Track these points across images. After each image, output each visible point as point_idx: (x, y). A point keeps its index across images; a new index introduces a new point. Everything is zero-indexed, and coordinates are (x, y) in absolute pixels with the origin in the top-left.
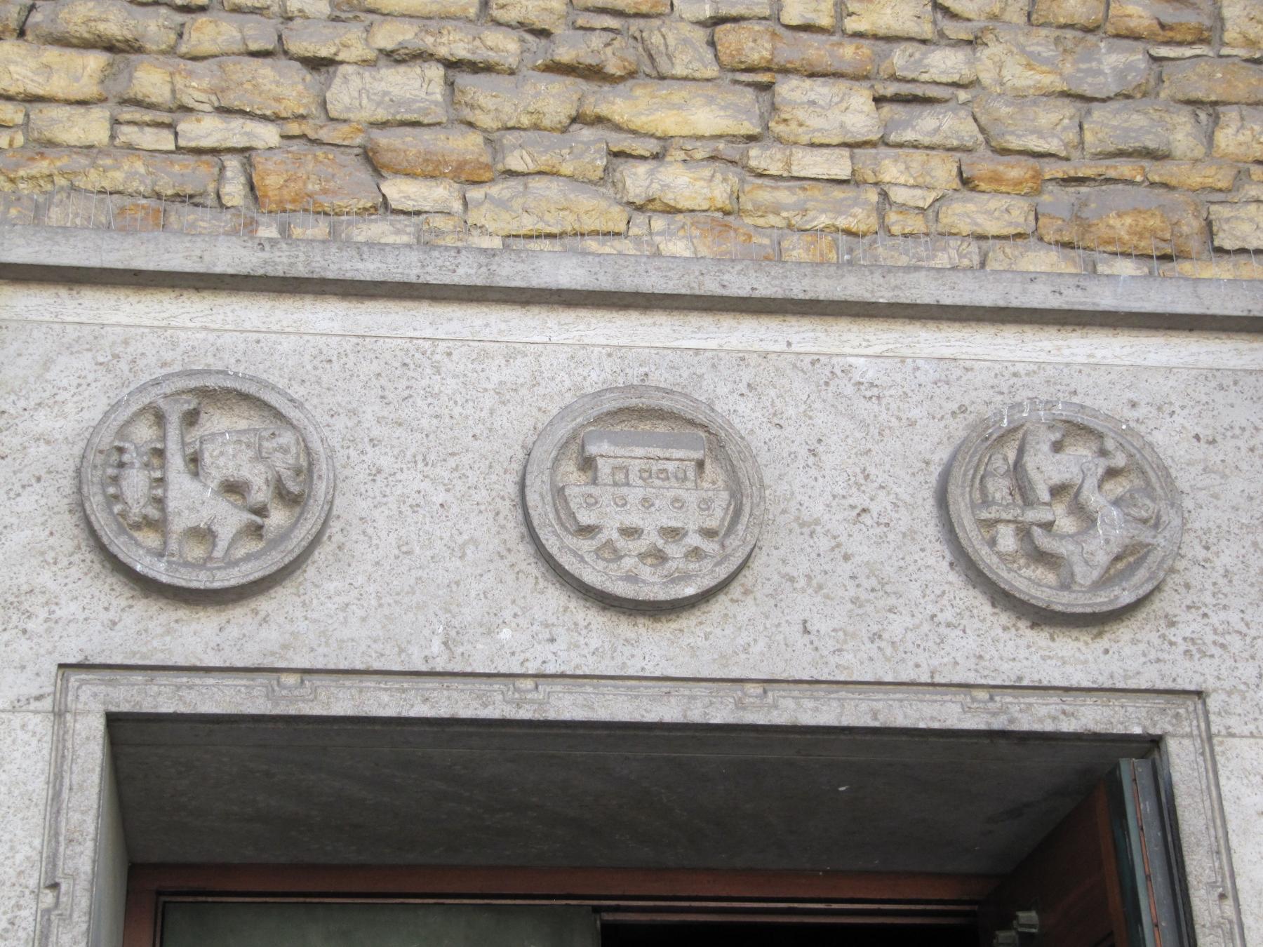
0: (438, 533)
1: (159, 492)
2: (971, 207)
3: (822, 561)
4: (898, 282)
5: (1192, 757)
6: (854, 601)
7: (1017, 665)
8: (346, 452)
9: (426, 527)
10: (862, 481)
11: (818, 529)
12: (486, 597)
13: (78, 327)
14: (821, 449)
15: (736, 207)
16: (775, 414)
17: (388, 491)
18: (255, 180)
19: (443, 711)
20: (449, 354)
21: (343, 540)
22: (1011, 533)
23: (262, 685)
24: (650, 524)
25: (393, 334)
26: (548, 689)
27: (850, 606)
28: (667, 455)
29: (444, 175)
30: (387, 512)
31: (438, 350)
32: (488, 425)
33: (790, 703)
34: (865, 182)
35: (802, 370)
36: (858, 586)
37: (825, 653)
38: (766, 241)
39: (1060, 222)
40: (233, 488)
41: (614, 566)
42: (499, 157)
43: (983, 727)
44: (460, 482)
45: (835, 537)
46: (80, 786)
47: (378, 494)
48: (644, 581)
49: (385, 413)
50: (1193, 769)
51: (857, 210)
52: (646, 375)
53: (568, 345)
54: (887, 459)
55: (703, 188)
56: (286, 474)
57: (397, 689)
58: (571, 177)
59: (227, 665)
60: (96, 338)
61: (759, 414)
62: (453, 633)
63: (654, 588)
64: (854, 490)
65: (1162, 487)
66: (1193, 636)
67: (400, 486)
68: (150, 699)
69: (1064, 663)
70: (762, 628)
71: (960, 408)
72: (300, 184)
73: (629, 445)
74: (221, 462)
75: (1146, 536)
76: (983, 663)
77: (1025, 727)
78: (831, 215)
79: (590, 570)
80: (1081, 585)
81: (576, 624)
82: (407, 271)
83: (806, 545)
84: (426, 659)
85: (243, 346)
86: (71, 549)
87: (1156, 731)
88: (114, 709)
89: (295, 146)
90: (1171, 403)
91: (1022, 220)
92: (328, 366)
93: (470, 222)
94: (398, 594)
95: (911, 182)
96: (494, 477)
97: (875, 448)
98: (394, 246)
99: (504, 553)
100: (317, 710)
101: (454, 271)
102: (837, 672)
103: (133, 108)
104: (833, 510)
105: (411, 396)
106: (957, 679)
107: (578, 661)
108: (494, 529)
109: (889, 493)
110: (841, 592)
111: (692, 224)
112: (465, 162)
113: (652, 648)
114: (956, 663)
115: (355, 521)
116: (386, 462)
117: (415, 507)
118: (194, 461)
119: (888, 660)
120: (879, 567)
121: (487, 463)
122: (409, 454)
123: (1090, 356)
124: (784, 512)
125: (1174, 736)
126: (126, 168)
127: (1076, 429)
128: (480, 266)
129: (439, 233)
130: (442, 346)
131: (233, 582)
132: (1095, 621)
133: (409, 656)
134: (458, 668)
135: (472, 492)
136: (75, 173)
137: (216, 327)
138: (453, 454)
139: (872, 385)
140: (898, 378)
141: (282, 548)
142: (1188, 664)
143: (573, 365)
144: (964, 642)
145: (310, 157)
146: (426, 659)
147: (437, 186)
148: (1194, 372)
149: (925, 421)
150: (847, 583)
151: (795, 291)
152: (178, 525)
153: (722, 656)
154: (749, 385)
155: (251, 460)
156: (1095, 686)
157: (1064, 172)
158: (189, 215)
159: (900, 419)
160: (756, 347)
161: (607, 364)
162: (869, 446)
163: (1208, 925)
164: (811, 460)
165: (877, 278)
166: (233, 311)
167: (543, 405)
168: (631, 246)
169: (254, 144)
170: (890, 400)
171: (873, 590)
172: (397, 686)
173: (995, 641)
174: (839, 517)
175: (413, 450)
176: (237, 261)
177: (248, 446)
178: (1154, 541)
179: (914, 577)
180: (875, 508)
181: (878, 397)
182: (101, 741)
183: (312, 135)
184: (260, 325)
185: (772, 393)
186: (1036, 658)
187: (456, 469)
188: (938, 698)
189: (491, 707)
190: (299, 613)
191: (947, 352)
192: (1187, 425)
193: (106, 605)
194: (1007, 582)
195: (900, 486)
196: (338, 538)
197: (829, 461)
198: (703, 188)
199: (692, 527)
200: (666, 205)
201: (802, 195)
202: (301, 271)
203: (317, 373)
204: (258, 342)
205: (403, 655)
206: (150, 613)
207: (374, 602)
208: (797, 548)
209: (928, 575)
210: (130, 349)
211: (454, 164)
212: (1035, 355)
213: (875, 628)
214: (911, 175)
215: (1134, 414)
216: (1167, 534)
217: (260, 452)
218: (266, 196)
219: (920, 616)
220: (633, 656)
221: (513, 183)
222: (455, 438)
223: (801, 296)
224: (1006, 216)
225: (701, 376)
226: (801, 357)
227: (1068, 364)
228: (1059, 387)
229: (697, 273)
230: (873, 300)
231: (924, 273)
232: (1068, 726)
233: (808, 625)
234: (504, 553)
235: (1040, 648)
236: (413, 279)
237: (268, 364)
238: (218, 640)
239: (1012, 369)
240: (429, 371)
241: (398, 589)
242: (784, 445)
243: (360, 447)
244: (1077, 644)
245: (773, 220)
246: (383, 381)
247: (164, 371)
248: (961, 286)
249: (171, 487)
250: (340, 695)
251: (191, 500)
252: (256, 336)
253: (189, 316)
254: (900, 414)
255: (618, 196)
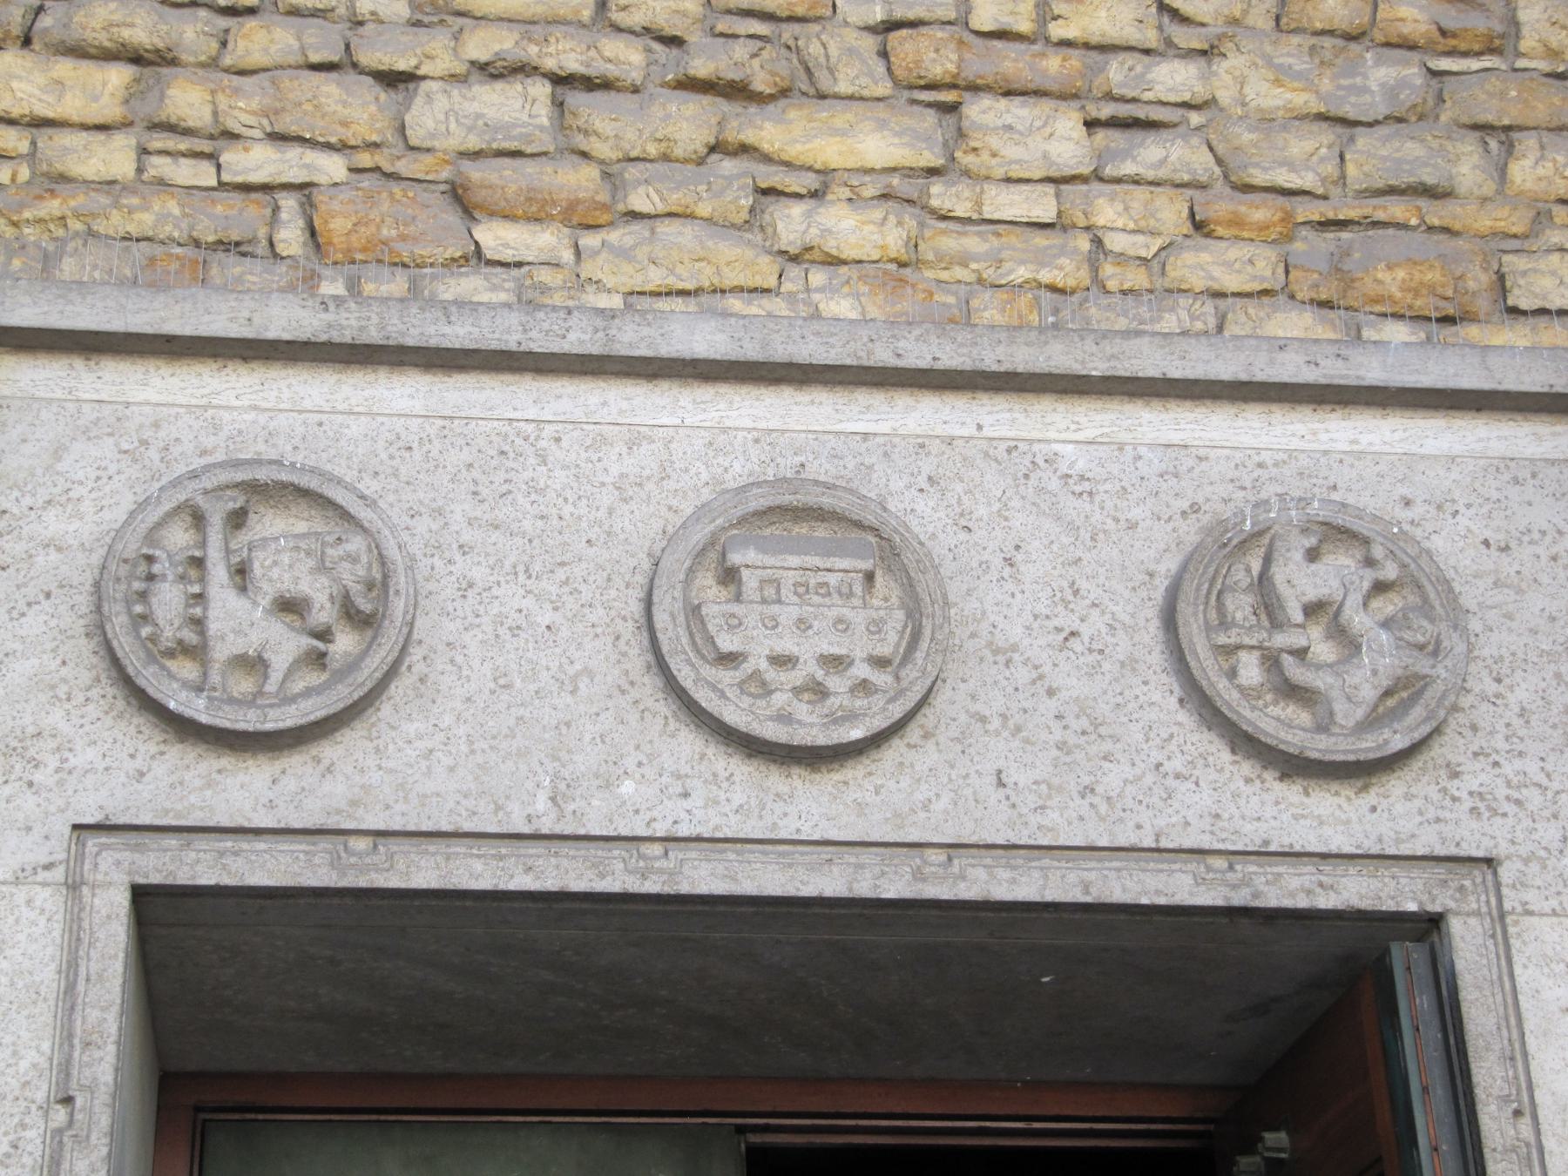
0: (544, 662)
1: (198, 611)
2: (1205, 257)
3: (1020, 696)
4: (1115, 350)
5: (1480, 940)
6: (1061, 746)
7: (1263, 826)
8: (429, 561)
9: (529, 655)
10: (1071, 598)
11: (1016, 656)
12: (603, 742)
13: (97, 406)
14: (1019, 557)
15: (913, 257)
16: (962, 515)
17: (482, 610)
18: (316, 224)
19: (550, 883)
20: (558, 440)
21: (426, 670)
22: (1256, 662)
23: (325, 851)
24: (807, 650)
25: (488, 414)
26: (681, 856)
27: (1055, 753)
28: (828, 566)
29: (551, 218)
30: (480, 636)
31: (544, 435)
32: (606, 527)
33: (981, 873)
34: (1074, 226)
35: (996, 460)
36: (1065, 727)
37: (1025, 811)
38: (951, 300)
39: (1316, 276)
40: (289, 606)
41: (762, 703)
42: (620, 195)
43: (1220, 902)
44: (571, 599)
45: (1036, 667)
46: (100, 976)
47: (469, 614)
48: (799, 722)
49: (478, 513)
50: (1481, 955)
51: (1064, 261)
52: (803, 465)
53: (705, 428)
54: (1101, 570)
55: (872, 233)
56: (356, 589)
57: (493, 856)
58: (709, 220)
59: (282, 825)
60: (119, 419)
61: (942, 514)
62: (562, 786)
63: (812, 730)
64: (1060, 608)
65: (1442, 605)
66: (1482, 789)
67: (496, 603)
68: (186, 868)
69: (1321, 823)
70: (945, 780)
71: (1191, 506)
72: (373, 229)
73: (781, 552)
74: (275, 573)
75: (1423, 666)
76: (1221, 824)
77: (1272, 902)
78: (1032, 267)
79: (732, 708)
80: (1342, 727)
81: (715, 775)
82: (505, 337)
83: (1000, 677)
84: (529, 818)
85: (302, 429)
86: (89, 682)
87: (1436, 908)
88: (141, 881)
89: (367, 182)
90: (1454, 501)
91: (1268, 273)
92: (407, 455)
93: (583, 276)
94: (494, 738)
95: (1132, 226)
96: (613, 593)
97: (1087, 556)
98: (490, 306)
99: (626, 687)
100: (394, 882)
101: (564, 337)
102: (1039, 834)
103: (165, 135)
104: (1035, 634)
105: (510, 492)
106: (1188, 843)
107: (716, 820)
108: (614, 657)
109: (1103, 613)
110: (1044, 735)
111: (860, 278)
112: (578, 202)
113: (810, 804)
114: (1187, 824)
115: (441, 647)
116: (479, 574)
117: (515, 630)
118: (241, 573)
119: (1102, 819)
120: (1092, 704)
121: (605, 574)
122: (508, 564)
123: (1353, 442)
124: (973, 635)
125: (1457, 914)
126: (156, 208)
127: (1336, 533)
128: (596, 331)
129: (545, 289)
130: (549, 430)
131: (289, 723)
132: (1360, 772)
133: (508, 814)
134: (568, 830)
135: (586, 610)
136: (93, 215)
137: (268, 405)
138: (562, 564)
139: (1082, 478)
140: (1115, 469)
141: (350, 680)
142: (1474, 825)
143: (711, 454)
144: (1196, 798)
145: (385, 195)
146: (529, 818)
147: (543, 231)
148: (1482, 462)
149: (1148, 522)
150: (1051, 724)
151: (987, 362)
152: (221, 652)
153: (897, 815)
154: (930, 478)
155: (312, 571)
156: (1359, 852)
157: (1321, 214)
158: (235, 267)
159: (1117, 520)
160: (938, 431)
161: (754, 452)
162: (1079, 554)
163: (1500, 1148)
164: (1007, 571)
165: (1089, 345)
166: (289, 386)
167: (674, 503)
168: (783, 305)
169: (315, 179)
170: (1105, 496)
171: (1084, 733)
172: (493, 852)
173: (1236, 796)
174: (1042, 642)
175: (513, 559)
176: (294, 324)
177: (308, 554)
178: (1432, 672)
179: (1135, 716)
180: (1086, 631)
181: (1091, 494)
182: (125, 920)
183: (388, 168)
184: (323, 403)
185: (959, 488)
186: (1285, 817)
187: (566, 582)
188: (1165, 866)
189: (609, 878)
190: (371, 762)
191: (1176, 438)
192: (1473, 528)
193: (132, 751)
194: (1250, 723)
195: (1117, 604)
196: (420, 668)
197: (1029, 572)
198: (872, 233)
199: (859, 654)
200: (827, 254)
201: (995, 242)
202: (374, 336)
203: (394, 463)
204: (320, 424)
205: (501, 814)
206: (186, 761)
207: (464, 748)
208: (989, 680)
209: (1152, 715)
210: (162, 434)
211: (564, 204)
212: (1285, 440)
213: (1086, 780)
214: (1131, 218)
215: (1408, 514)
216: (1449, 663)
217: (323, 561)
218: (330, 243)
219: (1143, 765)
220: (785, 815)
221: (637, 227)
222: (566, 544)
223: (995, 368)
224: (1249, 268)
225: (871, 467)
226: (995, 443)
227: (1326, 453)
228: (1314, 481)
229: (865, 339)
230: (1084, 372)
231: (1147, 339)
232: (1325, 902)
233: (1003, 776)
234: (626, 687)
235: (1292, 804)
236: (513, 347)
237: (332, 452)
238: (271, 795)
239: (1256, 459)
240: (532, 461)
241: (495, 731)
242: (973, 552)
243: (447, 555)
244: (1336, 800)
245: (959, 273)
246: (476, 474)
247: (203, 461)
248: (1193, 356)
249: (212, 605)
250: (423, 863)
251: (237, 621)
252: (317, 417)
253: (235, 393)
254: (1118, 514)
255: (768, 244)
